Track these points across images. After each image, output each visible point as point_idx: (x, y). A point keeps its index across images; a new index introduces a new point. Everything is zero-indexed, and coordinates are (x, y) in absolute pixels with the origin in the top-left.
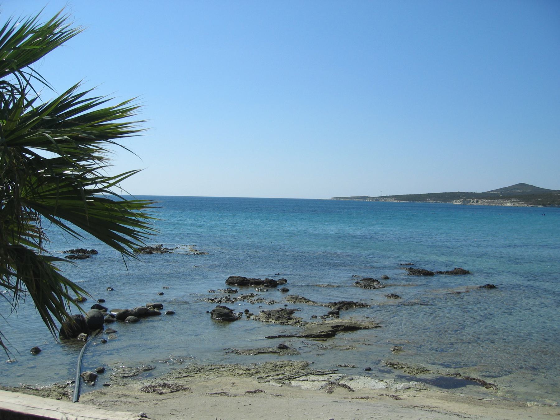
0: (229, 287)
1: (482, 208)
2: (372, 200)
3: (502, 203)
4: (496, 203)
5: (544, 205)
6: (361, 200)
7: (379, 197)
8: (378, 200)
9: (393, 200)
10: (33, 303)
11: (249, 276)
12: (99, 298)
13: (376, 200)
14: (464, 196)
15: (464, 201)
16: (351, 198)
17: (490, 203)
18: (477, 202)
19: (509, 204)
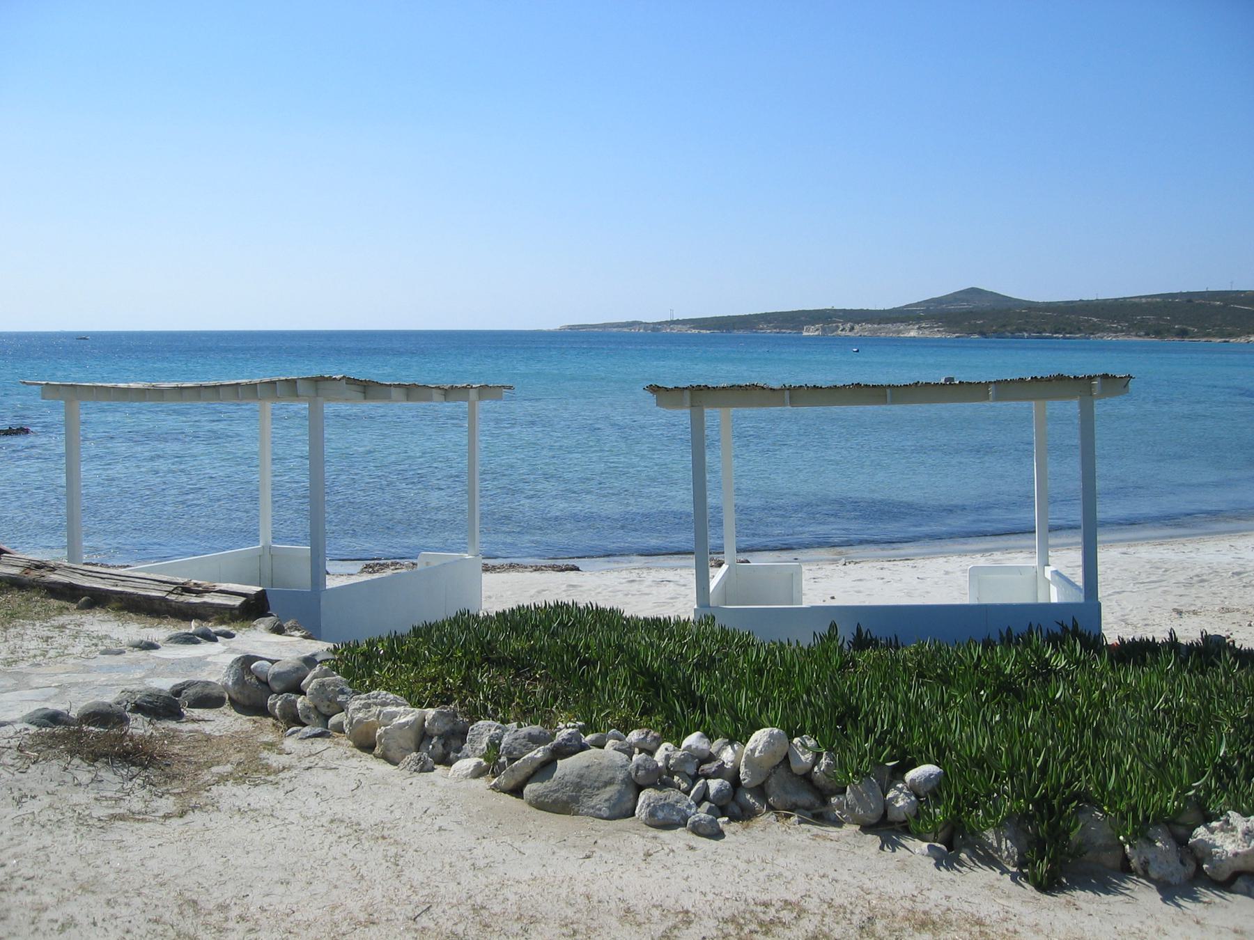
0: (466, 764)
1: (861, 342)
2: (645, 329)
3: (899, 332)
4: (888, 331)
5: (982, 334)
6: (626, 330)
7: (660, 323)
8: (658, 330)
9: (683, 329)
10: (1090, 894)
11: (612, 546)
12: (720, 843)
13: (654, 329)
14: (840, 317)
15: (823, 329)
16: (605, 326)
17: (875, 331)
18: (852, 329)
19: (913, 334)
